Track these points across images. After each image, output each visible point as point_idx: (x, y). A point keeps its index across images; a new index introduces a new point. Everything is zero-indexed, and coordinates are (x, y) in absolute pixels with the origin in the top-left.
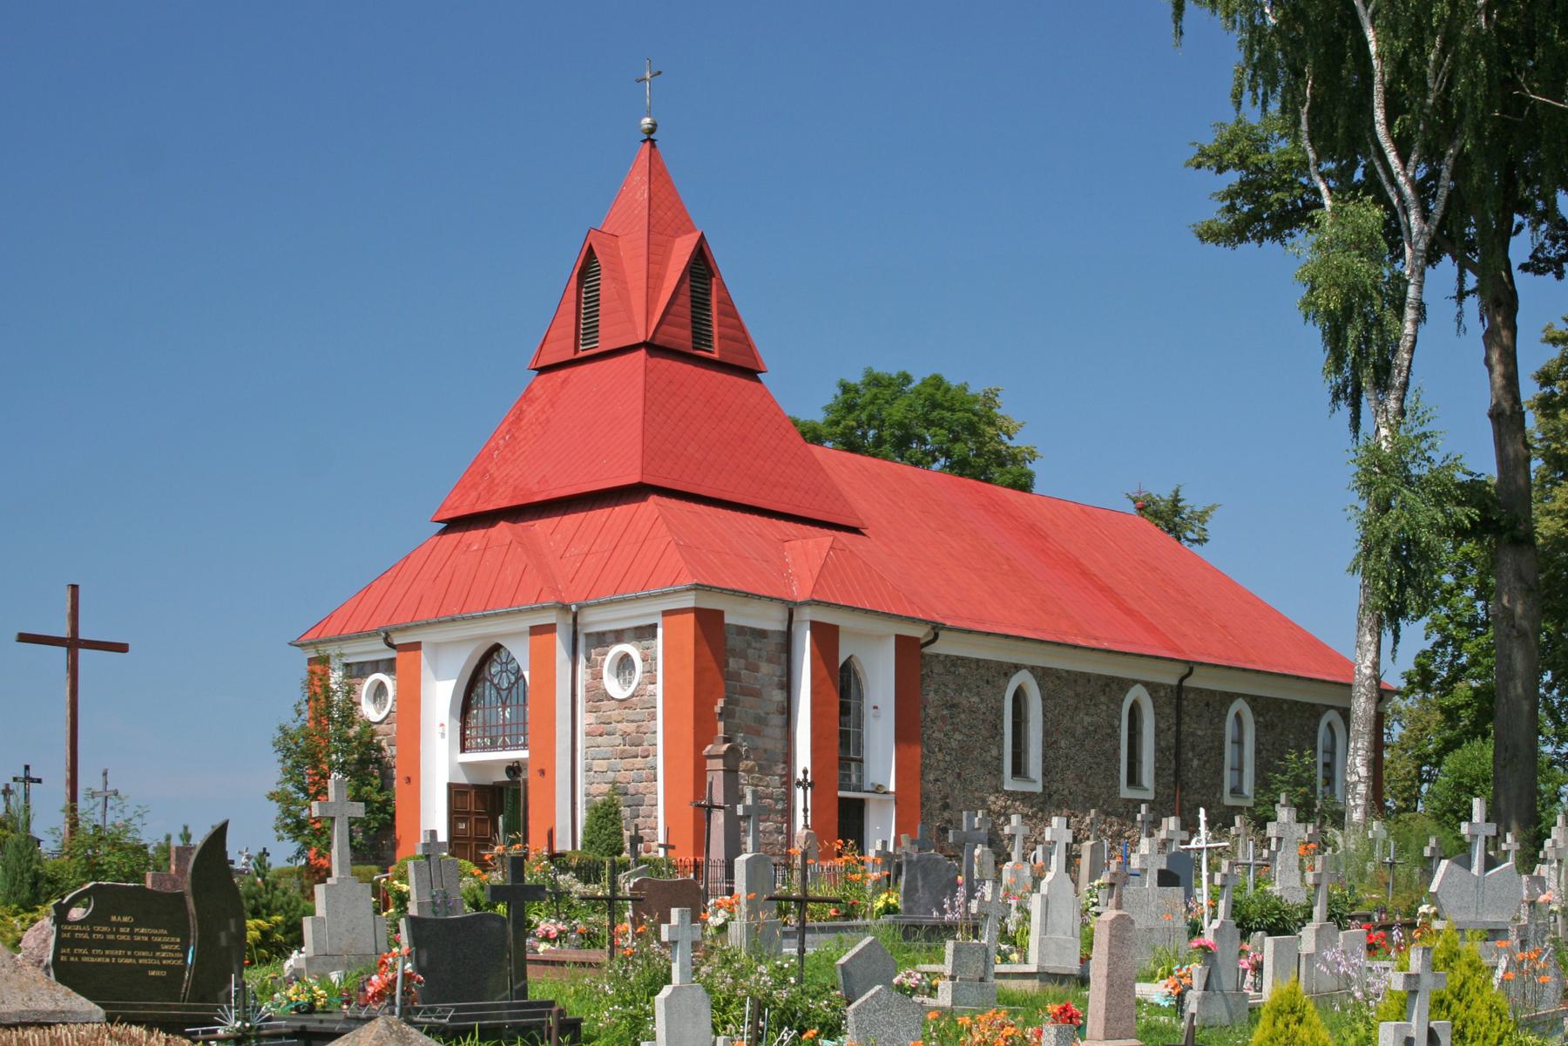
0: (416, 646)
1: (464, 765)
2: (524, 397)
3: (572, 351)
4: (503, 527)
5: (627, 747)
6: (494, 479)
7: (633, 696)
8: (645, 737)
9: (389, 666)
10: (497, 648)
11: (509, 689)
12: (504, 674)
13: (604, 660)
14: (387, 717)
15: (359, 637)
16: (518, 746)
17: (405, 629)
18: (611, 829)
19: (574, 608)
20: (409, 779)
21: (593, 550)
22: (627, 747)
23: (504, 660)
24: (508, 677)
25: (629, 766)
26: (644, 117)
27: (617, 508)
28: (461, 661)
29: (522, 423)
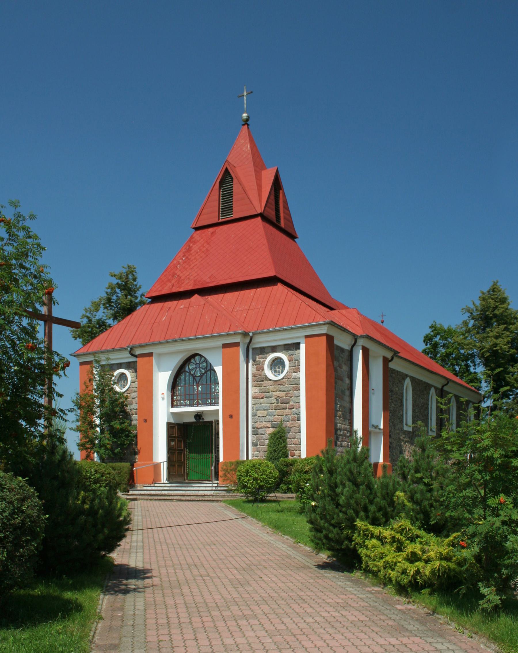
0: (150, 355)
1: (173, 414)
2: (190, 241)
3: (217, 218)
4: (196, 297)
5: (279, 404)
6: (180, 277)
7: (283, 378)
8: (291, 399)
9: (129, 366)
10: (194, 356)
11: (201, 376)
12: (198, 369)
13: (264, 361)
14: (127, 390)
15: (114, 351)
16: (206, 404)
17: (141, 346)
18: (283, 445)
19: (251, 334)
20: (231, 416)
21: (251, 307)
22: (279, 404)
23: (198, 362)
24: (200, 370)
25: (281, 413)
26: (244, 113)
27: (258, 289)
28: (175, 362)
29: (191, 252)
